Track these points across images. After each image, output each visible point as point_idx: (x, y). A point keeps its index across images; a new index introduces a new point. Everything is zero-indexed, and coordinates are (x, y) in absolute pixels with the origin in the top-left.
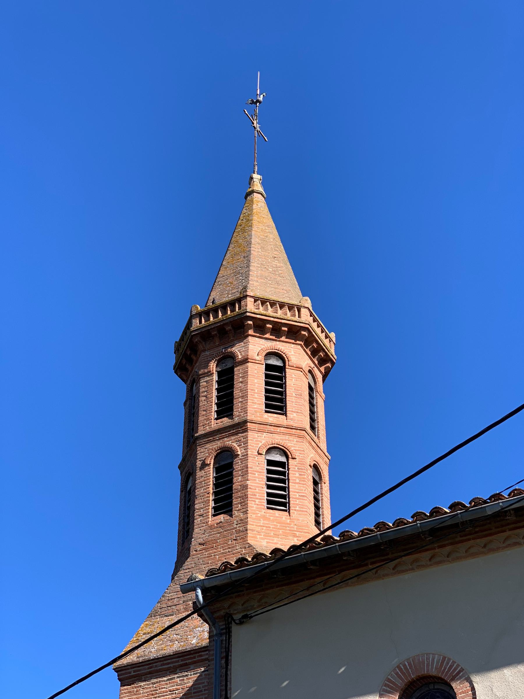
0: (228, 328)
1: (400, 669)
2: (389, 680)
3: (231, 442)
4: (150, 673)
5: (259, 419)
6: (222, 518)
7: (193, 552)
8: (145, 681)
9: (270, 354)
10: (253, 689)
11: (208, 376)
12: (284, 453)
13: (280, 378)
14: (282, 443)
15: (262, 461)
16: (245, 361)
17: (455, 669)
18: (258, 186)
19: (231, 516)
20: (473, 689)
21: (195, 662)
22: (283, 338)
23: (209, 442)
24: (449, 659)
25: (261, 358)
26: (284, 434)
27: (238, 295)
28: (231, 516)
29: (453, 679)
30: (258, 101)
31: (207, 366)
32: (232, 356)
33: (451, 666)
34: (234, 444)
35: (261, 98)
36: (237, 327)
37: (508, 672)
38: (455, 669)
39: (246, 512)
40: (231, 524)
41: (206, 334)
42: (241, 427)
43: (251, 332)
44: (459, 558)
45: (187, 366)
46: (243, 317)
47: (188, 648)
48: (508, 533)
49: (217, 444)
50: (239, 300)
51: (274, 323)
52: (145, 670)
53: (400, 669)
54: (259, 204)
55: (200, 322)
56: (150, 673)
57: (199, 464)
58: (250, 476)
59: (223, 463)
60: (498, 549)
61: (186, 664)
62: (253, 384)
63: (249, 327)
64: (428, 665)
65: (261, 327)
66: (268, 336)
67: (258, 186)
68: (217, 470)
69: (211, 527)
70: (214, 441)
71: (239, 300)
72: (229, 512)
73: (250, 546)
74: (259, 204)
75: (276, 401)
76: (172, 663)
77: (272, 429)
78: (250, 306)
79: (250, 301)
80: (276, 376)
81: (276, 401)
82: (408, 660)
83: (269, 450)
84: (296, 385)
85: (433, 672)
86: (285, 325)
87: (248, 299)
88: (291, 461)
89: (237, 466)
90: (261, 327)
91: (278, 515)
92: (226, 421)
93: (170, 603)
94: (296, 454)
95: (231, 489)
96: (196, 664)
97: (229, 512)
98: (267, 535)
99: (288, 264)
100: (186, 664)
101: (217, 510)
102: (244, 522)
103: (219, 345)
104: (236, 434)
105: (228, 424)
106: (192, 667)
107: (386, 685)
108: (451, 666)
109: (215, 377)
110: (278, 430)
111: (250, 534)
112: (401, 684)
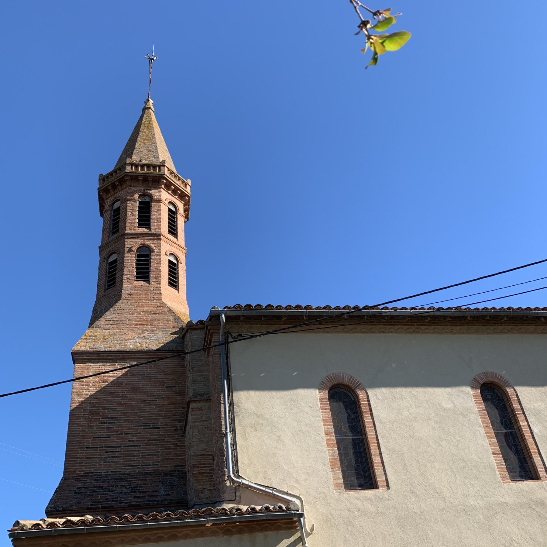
0: (150, 179)
1: (329, 378)
2: (323, 382)
3: (149, 242)
7: (123, 297)
8: (94, 363)
10: (243, 374)
11: (133, 201)
12: (177, 259)
14: (176, 253)
17: (357, 383)
19: (149, 283)
22: (177, 197)
24: (354, 378)
25: (167, 202)
28: (149, 283)
29: (356, 387)
30: (153, 59)
31: (133, 195)
32: (150, 196)
33: (355, 381)
34: (152, 245)
35: (155, 58)
38: (357, 383)
39: (159, 284)
41: (135, 178)
43: (163, 186)
44: (355, 332)
45: (111, 191)
46: (162, 176)
47: (128, 349)
48: (382, 326)
49: (141, 242)
50: (160, 167)
51: (175, 187)
52: (95, 357)
53: (329, 378)
55: (132, 169)
58: (162, 265)
59: (142, 253)
61: (125, 359)
63: (163, 183)
64: (343, 378)
66: (170, 192)
69: (135, 286)
70: (137, 239)
73: (163, 303)
75: (173, 230)
76: (115, 356)
82: (332, 374)
85: (346, 382)
86: (180, 190)
89: (153, 257)
91: (172, 290)
92: (145, 230)
93: (107, 322)
95: (148, 269)
100: (125, 359)
101: (138, 278)
105: (146, 232)
106: (128, 361)
107: (321, 384)
108: (355, 381)
110: (175, 245)
111: (163, 296)
112: (330, 385)
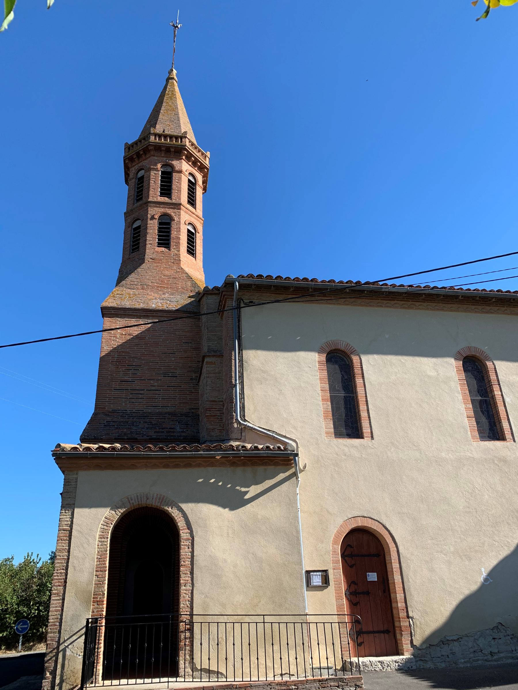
0: (172, 150)
4: (124, 315)
7: (146, 261)
14: (195, 223)
20: (360, 359)
21: (153, 316)
23: (157, 207)
24: (350, 345)
26: (195, 218)
28: (170, 250)
29: (351, 353)
30: (177, 27)
32: (172, 166)
33: (351, 348)
35: (179, 26)
37: (376, 356)
40: (170, 254)
41: (158, 148)
43: (184, 157)
45: (136, 159)
48: (380, 301)
50: (181, 138)
52: (122, 312)
55: (155, 139)
56: (124, 315)
57: (149, 216)
60: (373, 306)
65: (189, 157)
69: (157, 252)
71: (181, 138)
73: (182, 269)
75: (192, 201)
77: (191, 213)
82: (331, 341)
85: (343, 348)
86: (200, 162)
87: (187, 139)
88: (197, 233)
89: (174, 225)
92: (166, 199)
93: (132, 283)
96: (153, 317)
98: (188, 266)
100: (148, 316)
101: (160, 245)
103: (164, 157)
104: (174, 209)
108: (351, 348)
112: (328, 350)
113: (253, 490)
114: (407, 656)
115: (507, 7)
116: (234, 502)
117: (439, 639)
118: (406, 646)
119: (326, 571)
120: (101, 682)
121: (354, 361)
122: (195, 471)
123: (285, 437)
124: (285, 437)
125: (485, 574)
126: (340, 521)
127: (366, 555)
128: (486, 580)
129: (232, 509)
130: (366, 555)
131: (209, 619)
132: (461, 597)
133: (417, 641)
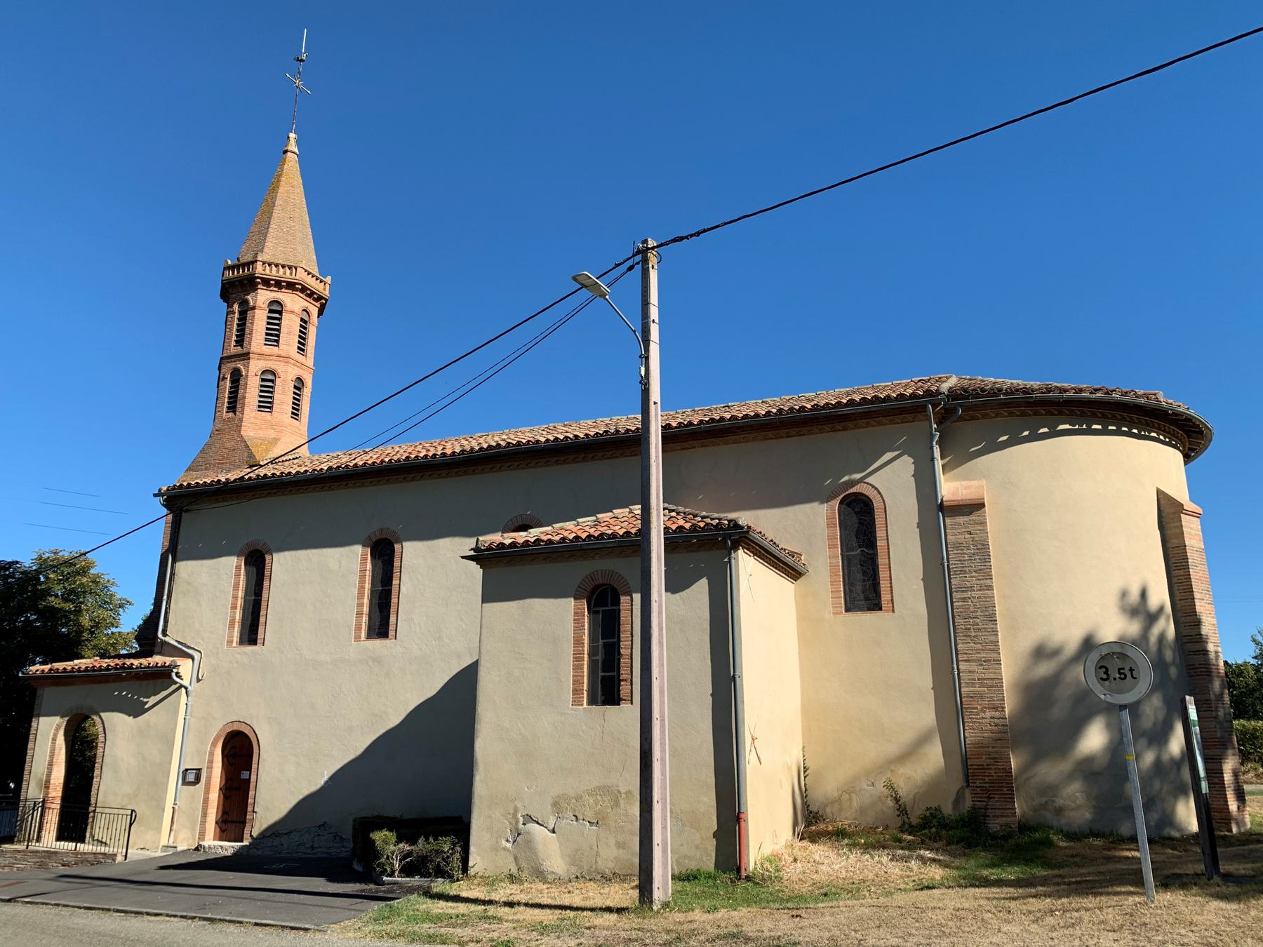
5: (258, 351)
6: (231, 414)
9: (272, 303)
12: (279, 303)
13: (278, 325)
15: (265, 313)
16: (254, 308)
18: (293, 146)
25: (265, 306)
27: (251, 259)
32: (247, 302)
36: (250, 283)
42: (245, 356)
49: (233, 365)
54: (292, 161)
62: (259, 321)
65: (266, 282)
67: (293, 146)
68: (232, 382)
72: (234, 412)
74: (292, 161)
78: (259, 269)
79: (259, 264)
80: (276, 310)
81: (273, 336)
83: (263, 372)
84: (290, 325)
90: (266, 282)
94: (281, 374)
97: (234, 412)
99: (1077, 902)
102: (241, 420)
109: (237, 315)
112: (246, 552)
113: (152, 700)
114: (246, 843)
115: (322, 788)
116: (137, 710)
117: (273, 832)
118: (246, 835)
119: (199, 770)
120: (49, 840)
121: (621, 512)
122: (113, 685)
123: (189, 647)
124: (189, 647)
125: (326, 778)
126: (220, 726)
127: (239, 750)
128: (326, 783)
129: (135, 717)
130: (239, 750)
131: (107, 811)
132: (301, 797)
133: (255, 834)
